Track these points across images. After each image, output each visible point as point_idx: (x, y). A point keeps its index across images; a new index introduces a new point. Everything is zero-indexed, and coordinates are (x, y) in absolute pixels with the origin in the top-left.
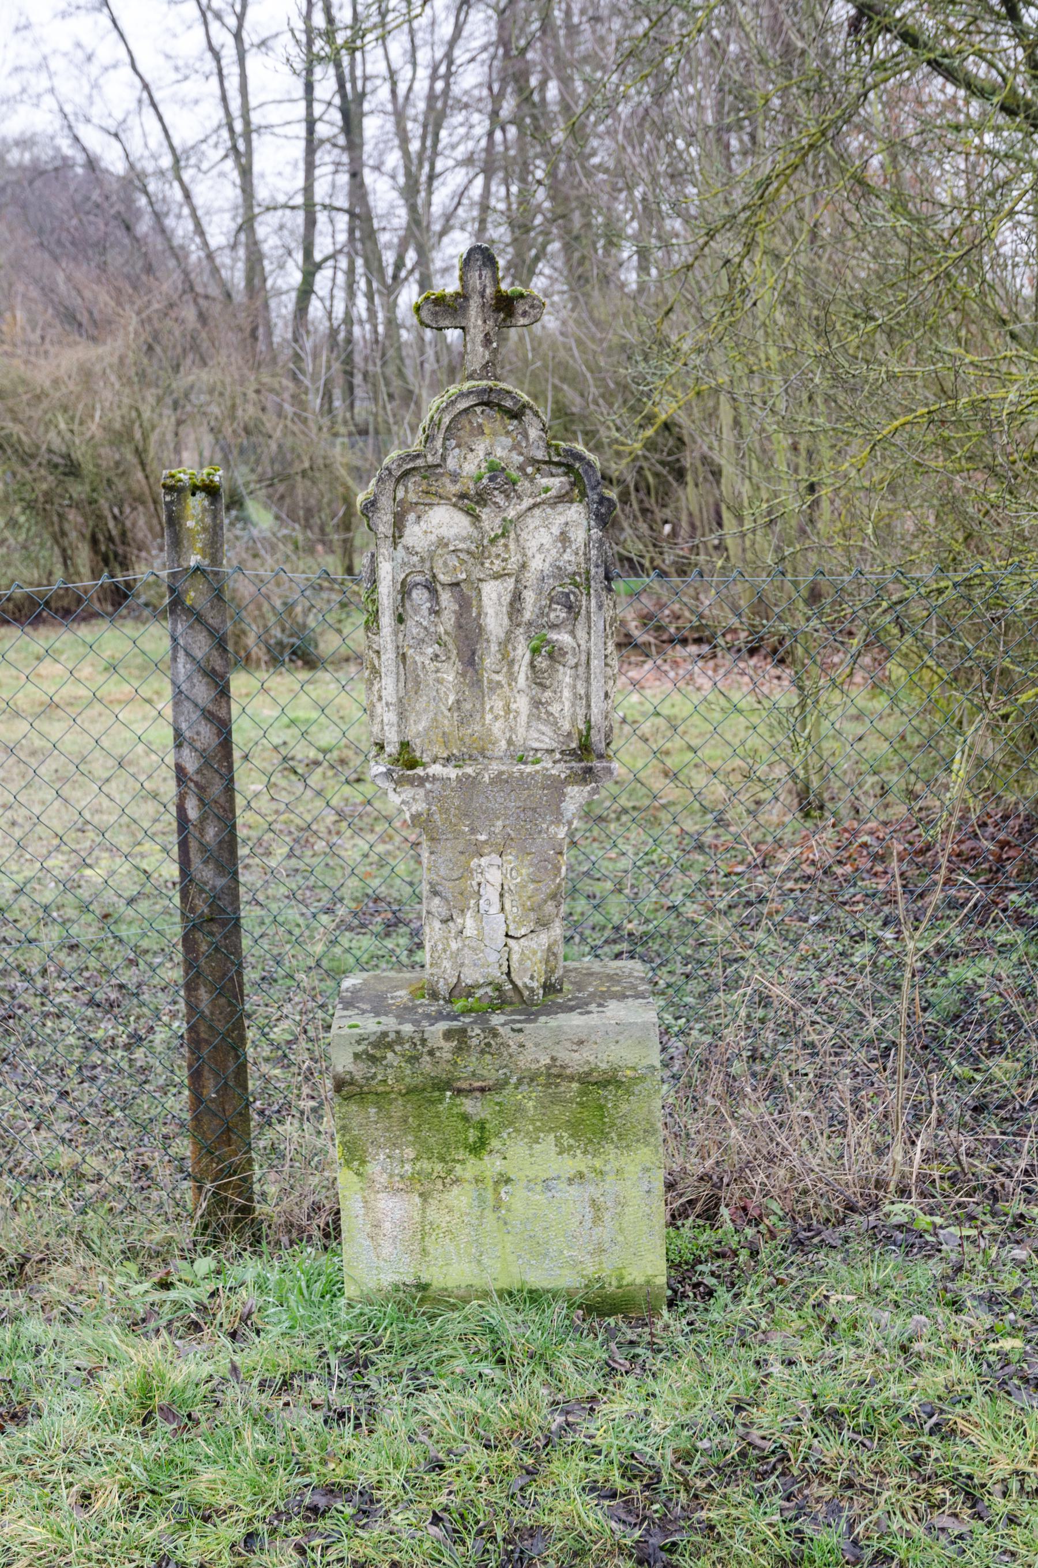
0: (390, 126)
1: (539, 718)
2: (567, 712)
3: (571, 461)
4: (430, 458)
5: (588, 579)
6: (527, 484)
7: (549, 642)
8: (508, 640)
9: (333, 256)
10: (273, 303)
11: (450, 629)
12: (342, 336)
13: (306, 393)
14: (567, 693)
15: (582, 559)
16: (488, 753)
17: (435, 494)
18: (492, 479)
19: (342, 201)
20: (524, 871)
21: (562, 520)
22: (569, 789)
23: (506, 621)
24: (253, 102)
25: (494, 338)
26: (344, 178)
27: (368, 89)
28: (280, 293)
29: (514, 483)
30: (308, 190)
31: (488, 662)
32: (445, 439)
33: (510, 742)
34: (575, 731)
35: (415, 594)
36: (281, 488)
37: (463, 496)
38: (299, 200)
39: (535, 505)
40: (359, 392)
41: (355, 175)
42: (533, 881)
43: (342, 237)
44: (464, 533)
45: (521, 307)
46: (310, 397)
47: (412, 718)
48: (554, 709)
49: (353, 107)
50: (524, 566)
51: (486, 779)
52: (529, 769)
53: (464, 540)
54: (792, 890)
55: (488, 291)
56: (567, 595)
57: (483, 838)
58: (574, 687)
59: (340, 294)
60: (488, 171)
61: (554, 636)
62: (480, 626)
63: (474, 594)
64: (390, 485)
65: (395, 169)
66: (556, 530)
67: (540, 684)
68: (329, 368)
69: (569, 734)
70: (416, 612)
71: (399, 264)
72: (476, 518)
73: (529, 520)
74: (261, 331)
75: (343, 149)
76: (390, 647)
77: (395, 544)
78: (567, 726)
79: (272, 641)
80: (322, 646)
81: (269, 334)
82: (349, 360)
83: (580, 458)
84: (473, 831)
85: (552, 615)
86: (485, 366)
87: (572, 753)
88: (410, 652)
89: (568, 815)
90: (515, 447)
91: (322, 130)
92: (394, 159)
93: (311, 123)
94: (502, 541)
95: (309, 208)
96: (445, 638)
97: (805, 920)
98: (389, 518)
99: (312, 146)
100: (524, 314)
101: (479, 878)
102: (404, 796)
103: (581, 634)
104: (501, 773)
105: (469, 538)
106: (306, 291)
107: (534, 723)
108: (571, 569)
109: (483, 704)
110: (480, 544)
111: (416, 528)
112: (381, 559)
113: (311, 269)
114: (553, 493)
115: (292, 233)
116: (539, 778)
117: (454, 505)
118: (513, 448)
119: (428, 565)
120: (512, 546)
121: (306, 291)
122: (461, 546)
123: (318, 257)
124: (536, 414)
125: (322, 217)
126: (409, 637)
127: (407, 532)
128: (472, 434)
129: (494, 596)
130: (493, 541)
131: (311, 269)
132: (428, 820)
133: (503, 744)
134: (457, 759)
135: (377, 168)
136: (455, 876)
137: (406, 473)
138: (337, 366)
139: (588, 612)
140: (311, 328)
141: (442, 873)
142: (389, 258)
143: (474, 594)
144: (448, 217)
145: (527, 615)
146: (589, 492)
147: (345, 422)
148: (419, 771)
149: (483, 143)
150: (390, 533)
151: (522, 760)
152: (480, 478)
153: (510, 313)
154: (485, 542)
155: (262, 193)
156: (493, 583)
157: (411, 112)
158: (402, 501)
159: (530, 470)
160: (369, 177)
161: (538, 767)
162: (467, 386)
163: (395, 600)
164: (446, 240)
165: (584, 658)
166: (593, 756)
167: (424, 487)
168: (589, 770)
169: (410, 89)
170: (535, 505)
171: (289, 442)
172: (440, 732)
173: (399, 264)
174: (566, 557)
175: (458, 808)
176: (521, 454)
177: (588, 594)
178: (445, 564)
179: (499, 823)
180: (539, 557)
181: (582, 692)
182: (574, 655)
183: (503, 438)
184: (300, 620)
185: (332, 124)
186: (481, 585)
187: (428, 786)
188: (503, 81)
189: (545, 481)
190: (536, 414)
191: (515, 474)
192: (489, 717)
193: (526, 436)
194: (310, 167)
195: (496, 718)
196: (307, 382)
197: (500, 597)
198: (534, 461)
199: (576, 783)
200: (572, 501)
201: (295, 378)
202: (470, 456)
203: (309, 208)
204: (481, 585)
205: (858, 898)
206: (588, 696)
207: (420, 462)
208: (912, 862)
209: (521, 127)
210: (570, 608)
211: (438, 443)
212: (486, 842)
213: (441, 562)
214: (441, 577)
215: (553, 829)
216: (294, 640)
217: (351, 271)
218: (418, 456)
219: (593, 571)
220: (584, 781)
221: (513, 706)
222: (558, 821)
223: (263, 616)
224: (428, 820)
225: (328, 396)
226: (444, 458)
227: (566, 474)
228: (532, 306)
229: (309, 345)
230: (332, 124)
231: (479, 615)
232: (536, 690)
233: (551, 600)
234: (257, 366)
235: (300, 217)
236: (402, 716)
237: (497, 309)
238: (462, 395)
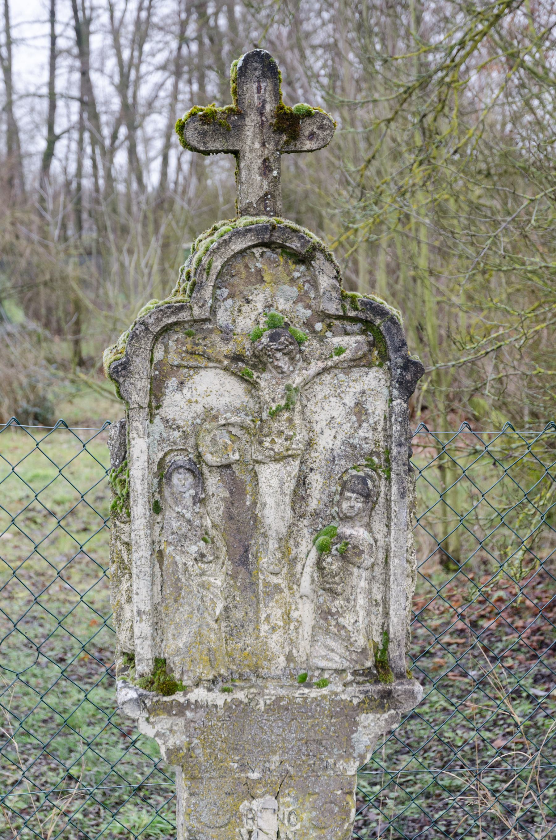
0: (109, 40)
1: (327, 632)
2: (361, 625)
3: (370, 316)
4: (196, 311)
5: (387, 460)
6: (315, 343)
7: (340, 538)
8: (290, 534)
9: (68, 131)
10: (25, 162)
11: (217, 520)
12: (74, 186)
13: (48, 224)
14: (361, 601)
15: (381, 436)
16: (262, 672)
17: (203, 355)
18: (273, 338)
19: (75, 92)
20: (305, 816)
21: (358, 387)
22: (362, 717)
23: (289, 513)
24: (13, 22)
25: (274, 165)
26: (77, 76)
27: (94, 15)
28: (30, 155)
29: (300, 343)
30: (51, 84)
31: (264, 561)
32: (216, 287)
33: (289, 658)
34: (370, 646)
35: (176, 479)
36: (29, 295)
37: (237, 358)
38: (45, 91)
39: (326, 370)
40: (86, 225)
41: (85, 73)
42: (317, 827)
43: (75, 118)
44: (237, 403)
45: (307, 127)
46: (51, 228)
47: (171, 631)
48: (347, 620)
49: (83, 28)
50: (310, 444)
51: (261, 706)
52: (314, 693)
53: (237, 411)
54: (449, 644)
55: (268, 107)
56: (363, 480)
57: (255, 776)
58: (370, 591)
59: (73, 157)
60: (178, 74)
61: (346, 530)
62: (255, 518)
63: (248, 478)
64: (146, 344)
65: (113, 71)
66: (350, 401)
67: (330, 591)
68: (65, 207)
69: (364, 650)
70: (177, 501)
71: (114, 137)
72: (253, 385)
73: (317, 388)
74: (16, 182)
75: (76, 57)
76: (144, 542)
77: (151, 416)
78: (361, 641)
79: (20, 410)
80: (57, 413)
81: (23, 184)
82: (79, 201)
83: (381, 312)
84: (243, 767)
85: (345, 505)
86: (264, 198)
87: (367, 673)
88: (169, 550)
89: (360, 748)
90: (301, 298)
91: (61, 43)
92: (111, 64)
93: (53, 38)
94: (286, 415)
95: (52, 97)
96: (213, 532)
97: (465, 675)
98: (145, 384)
99: (54, 54)
100: (312, 136)
101: (250, 825)
102: (158, 727)
103: (379, 526)
104: (280, 698)
105: (242, 409)
106: (49, 155)
107: (321, 638)
108: (367, 448)
109: (257, 612)
110: (257, 417)
111: (178, 397)
112: (133, 434)
113: (52, 139)
114: (347, 355)
115: (40, 113)
116: (326, 704)
117: (226, 369)
118: (299, 299)
119: (192, 441)
120: (297, 421)
121: (49, 155)
122: (234, 419)
123: (58, 130)
124: (329, 258)
125: (60, 103)
126: (167, 532)
127: (167, 401)
128: (248, 282)
129: (275, 482)
130: (274, 415)
131: (52, 139)
132: (188, 756)
133: (282, 661)
134: (224, 680)
135: (101, 71)
136: (220, 822)
137: (167, 329)
138: (70, 207)
139: (388, 501)
140: (52, 179)
141: (205, 818)
142: (106, 132)
143: (248, 478)
144: (150, 105)
145: (313, 504)
146: (392, 356)
147: (76, 247)
148: (179, 697)
149: (175, 53)
150: (145, 402)
151: (304, 681)
152: (258, 336)
153: (294, 136)
154: (265, 415)
155: (19, 85)
156: (273, 466)
157: (123, 31)
158: (160, 362)
159: (319, 326)
160: (94, 76)
161: (325, 691)
162: (243, 222)
163: (150, 485)
164: (148, 119)
165: (381, 555)
166: (392, 677)
167: (189, 346)
168: (387, 694)
169: (123, 17)
170: (326, 370)
171: (35, 259)
172: (205, 647)
173: (114, 137)
174: (362, 433)
175: (226, 741)
176: (309, 307)
177: (388, 479)
178: (214, 441)
179: (276, 758)
180: (329, 433)
181: (379, 597)
182: (371, 554)
183: (286, 288)
184: (41, 393)
185: (68, 38)
186: (259, 468)
187: (189, 714)
188: (188, 11)
189: (337, 341)
190: (329, 258)
191: (301, 332)
192: (264, 628)
193: (315, 285)
194: (53, 68)
195: (274, 629)
196: (48, 217)
197: (282, 484)
198: (324, 316)
199: (372, 710)
200: (369, 365)
201: (41, 217)
202: (246, 308)
203: (52, 97)
204: (259, 468)
205: (507, 653)
206: (385, 602)
207: (184, 316)
208: (544, 617)
209: (201, 44)
210: (367, 496)
211: (207, 292)
212: (259, 781)
213: (208, 438)
214: (209, 458)
215: (341, 765)
216: (37, 410)
217: (81, 142)
218: (181, 308)
219: (395, 451)
220: (382, 708)
221: (295, 615)
222: (348, 755)
223: (13, 391)
224: (188, 756)
225: (64, 227)
226: (213, 311)
227: (363, 332)
228: (321, 127)
229: (50, 191)
230: (68, 38)
231: (254, 503)
232: (324, 597)
233: (344, 485)
234: (13, 206)
235: (44, 105)
236: (157, 626)
237: (279, 130)
238: (238, 234)
